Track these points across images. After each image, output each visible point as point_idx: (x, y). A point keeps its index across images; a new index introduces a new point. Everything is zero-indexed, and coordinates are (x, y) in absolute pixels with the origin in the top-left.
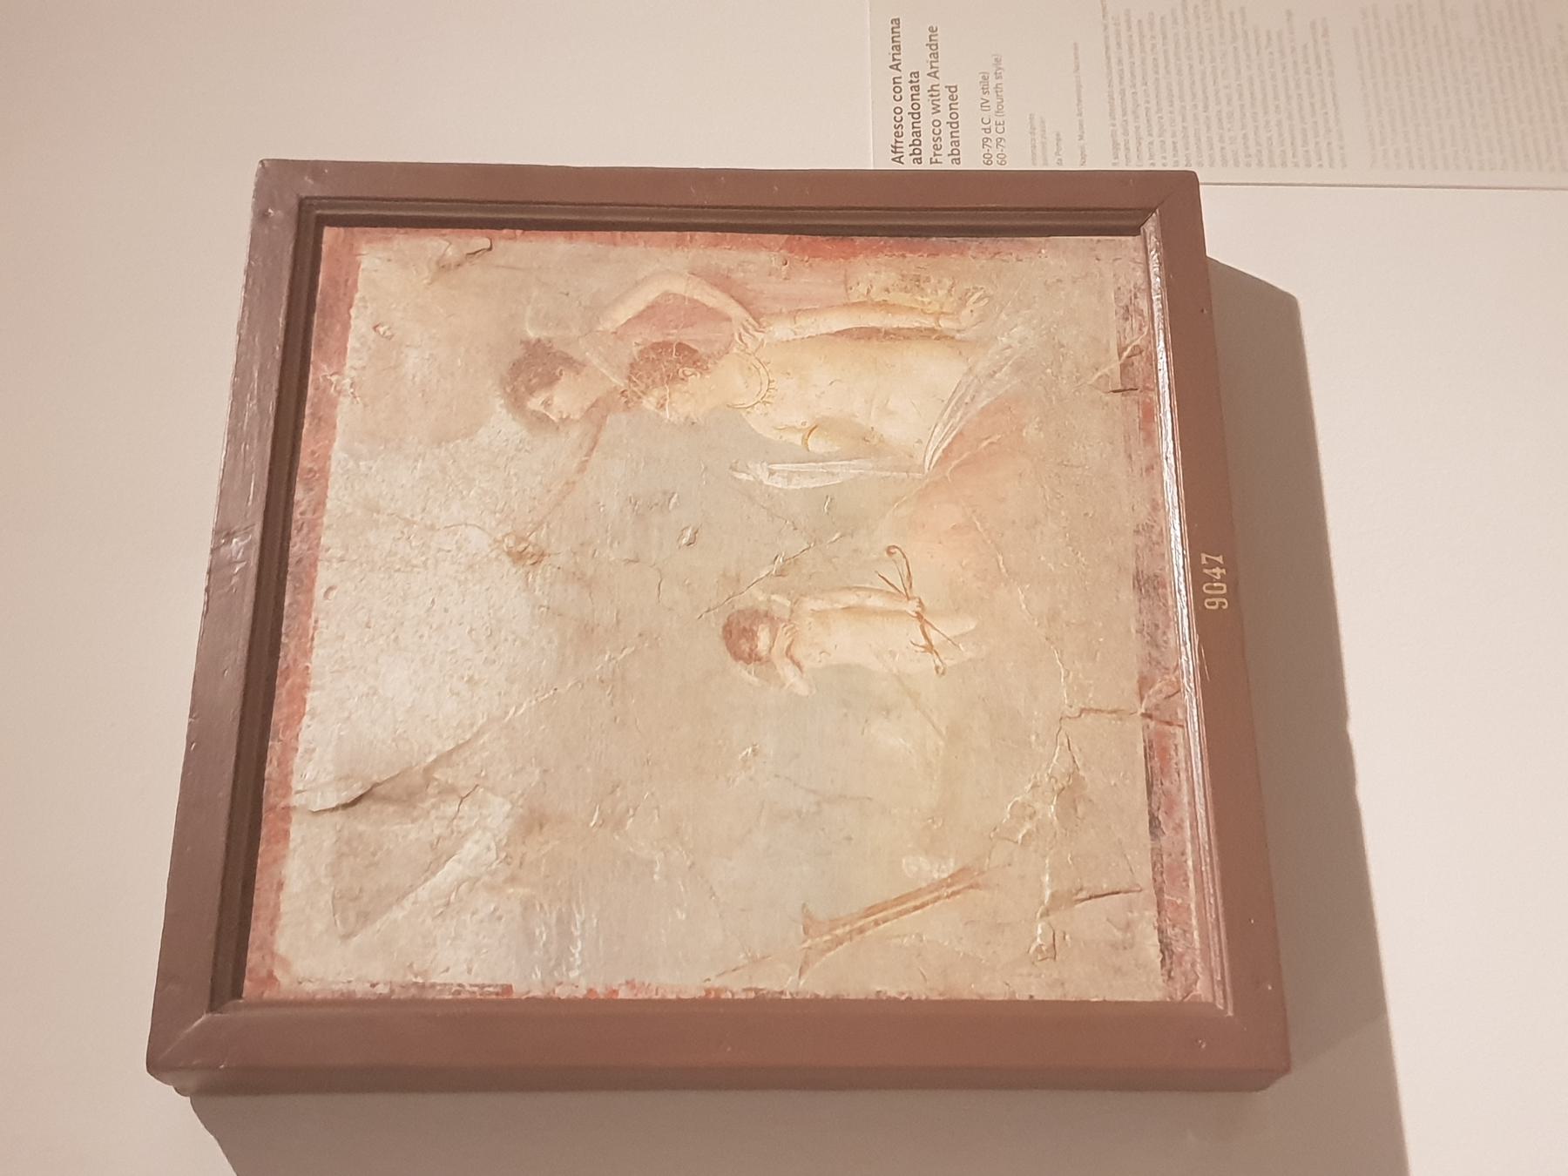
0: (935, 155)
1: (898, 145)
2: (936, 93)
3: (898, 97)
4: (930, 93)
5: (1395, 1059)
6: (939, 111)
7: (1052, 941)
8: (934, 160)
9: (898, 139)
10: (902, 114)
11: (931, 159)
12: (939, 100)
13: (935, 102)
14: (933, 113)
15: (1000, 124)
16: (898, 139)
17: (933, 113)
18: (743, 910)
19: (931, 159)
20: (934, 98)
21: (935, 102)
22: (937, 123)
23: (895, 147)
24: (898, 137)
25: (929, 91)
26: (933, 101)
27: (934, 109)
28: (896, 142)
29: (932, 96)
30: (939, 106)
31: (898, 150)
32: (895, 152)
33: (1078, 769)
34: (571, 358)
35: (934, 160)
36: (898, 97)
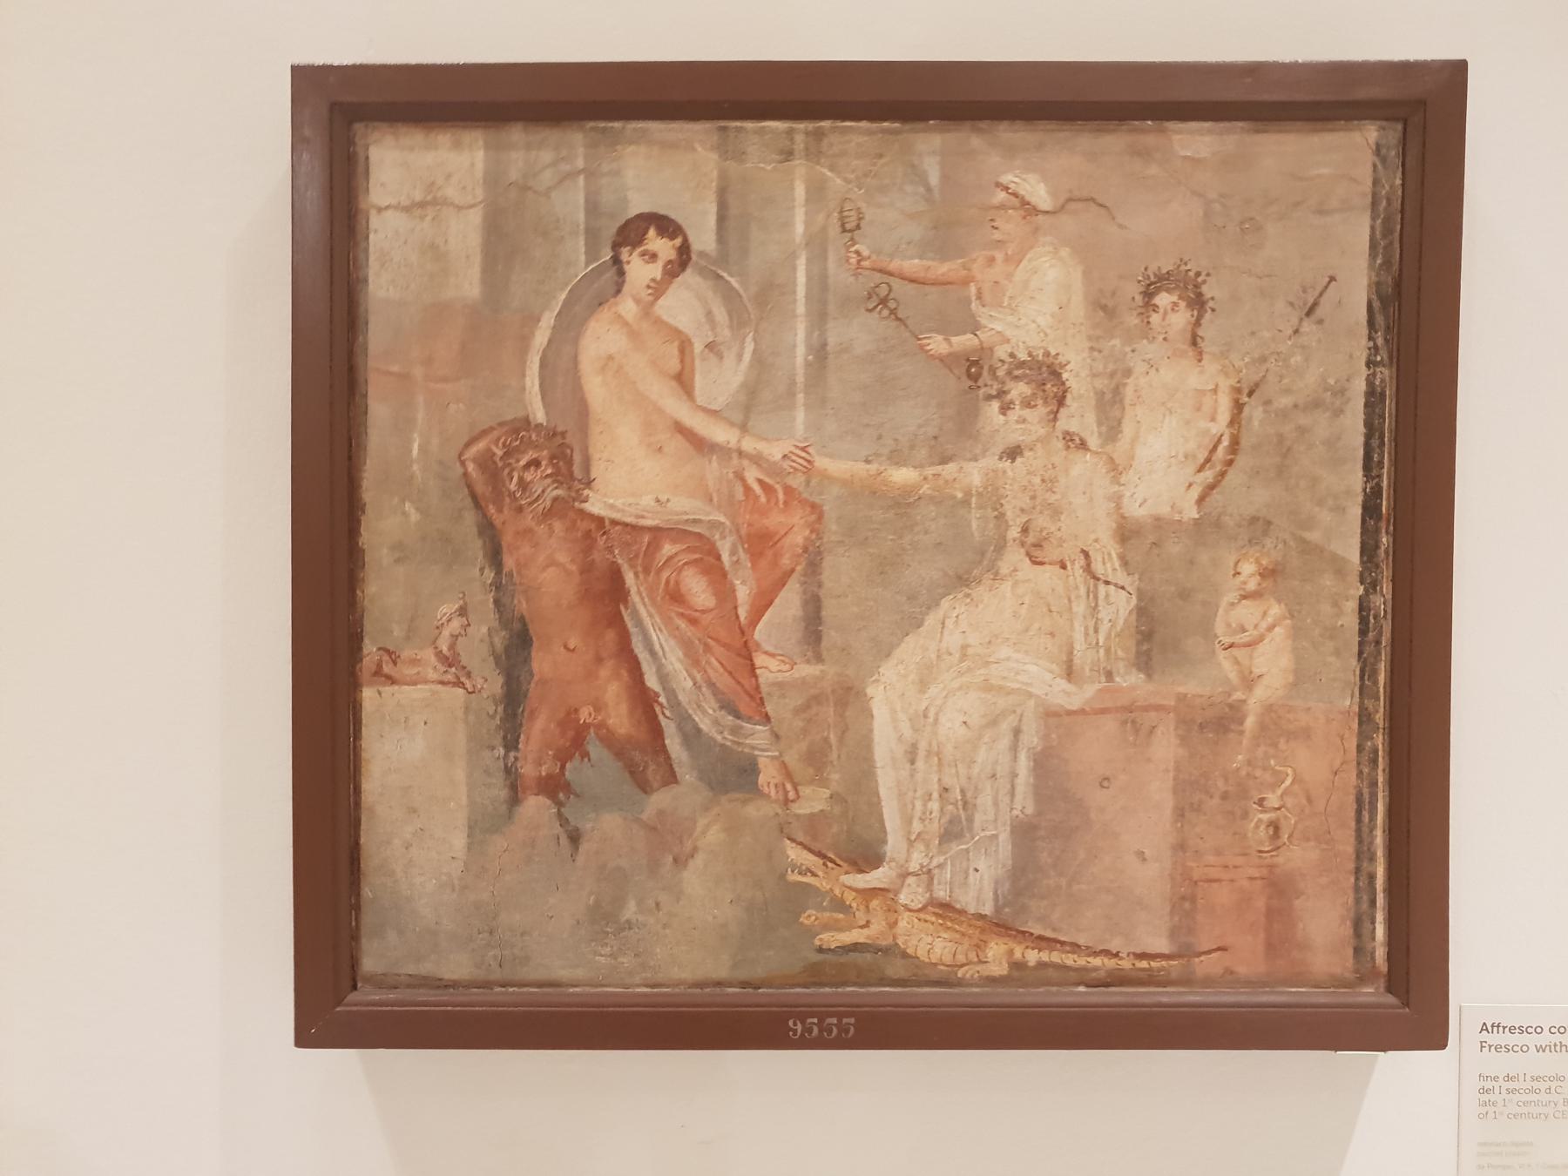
0: (1490, 1046)
1: (1501, 1029)
2: (1558, 1048)
3: (1553, 1030)
4: (1559, 1044)
5: (363, 770)
6: (1538, 1051)
7: (1202, 950)
8: (1484, 1044)
9: (1507, 1029)
10: (1558, 1033)
11: (1486, 1042)
12: (1551, 1051)
13: (1548, 1048)
14: (1536, 1046)
15: (1563, 1114)
16: (1507, 1029)
17: (1536, 1046)
18: (1073, 417)
19: (1486, 1042)
20: (1553, 1047)
21: (1548, 1048)
22: (1525, 1049)
23: (1498, 1026)
24: (1510, 1029)
25: (1561, 1042)
26: (1550, 1046)
27: (1541, 1046)
28: (1504, 1028)
29: (1555, 1045)
30: (1544, 1051)
31: (1495, 1029)
32: (1493, 1026)
33: (638, 504)
34: (568, 837)
35: (1484, 1044)
36: (1539, 1030)
